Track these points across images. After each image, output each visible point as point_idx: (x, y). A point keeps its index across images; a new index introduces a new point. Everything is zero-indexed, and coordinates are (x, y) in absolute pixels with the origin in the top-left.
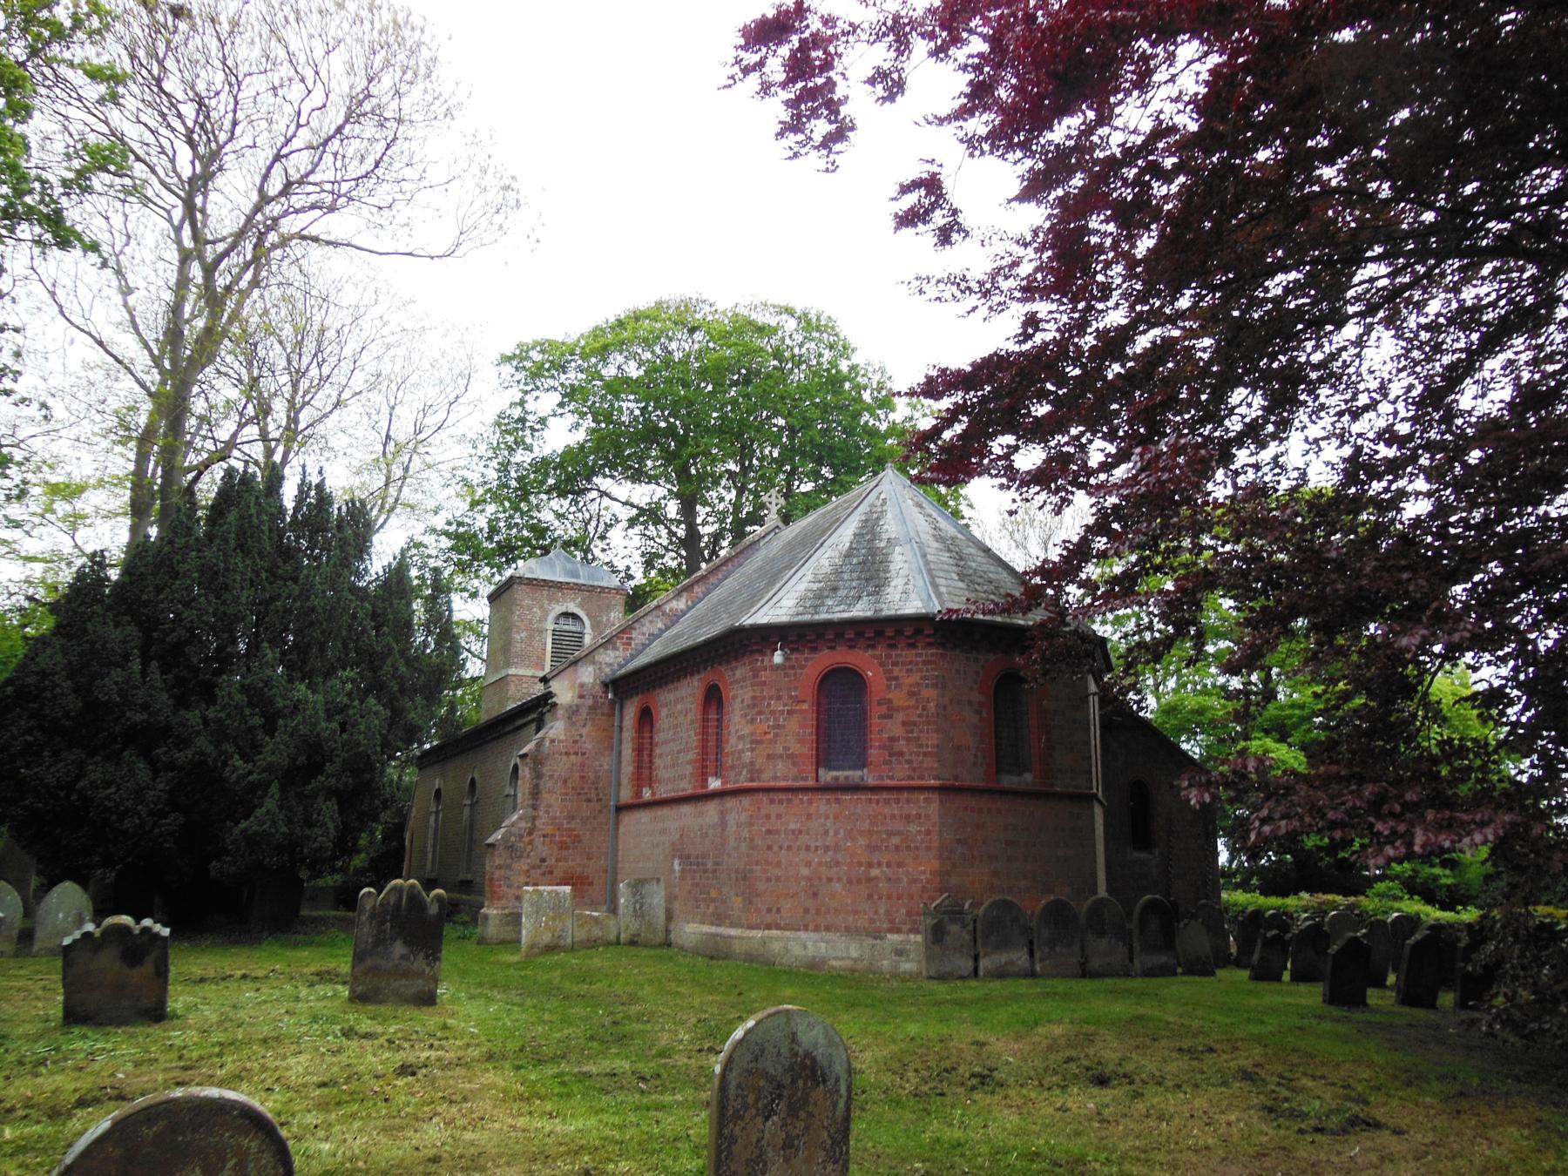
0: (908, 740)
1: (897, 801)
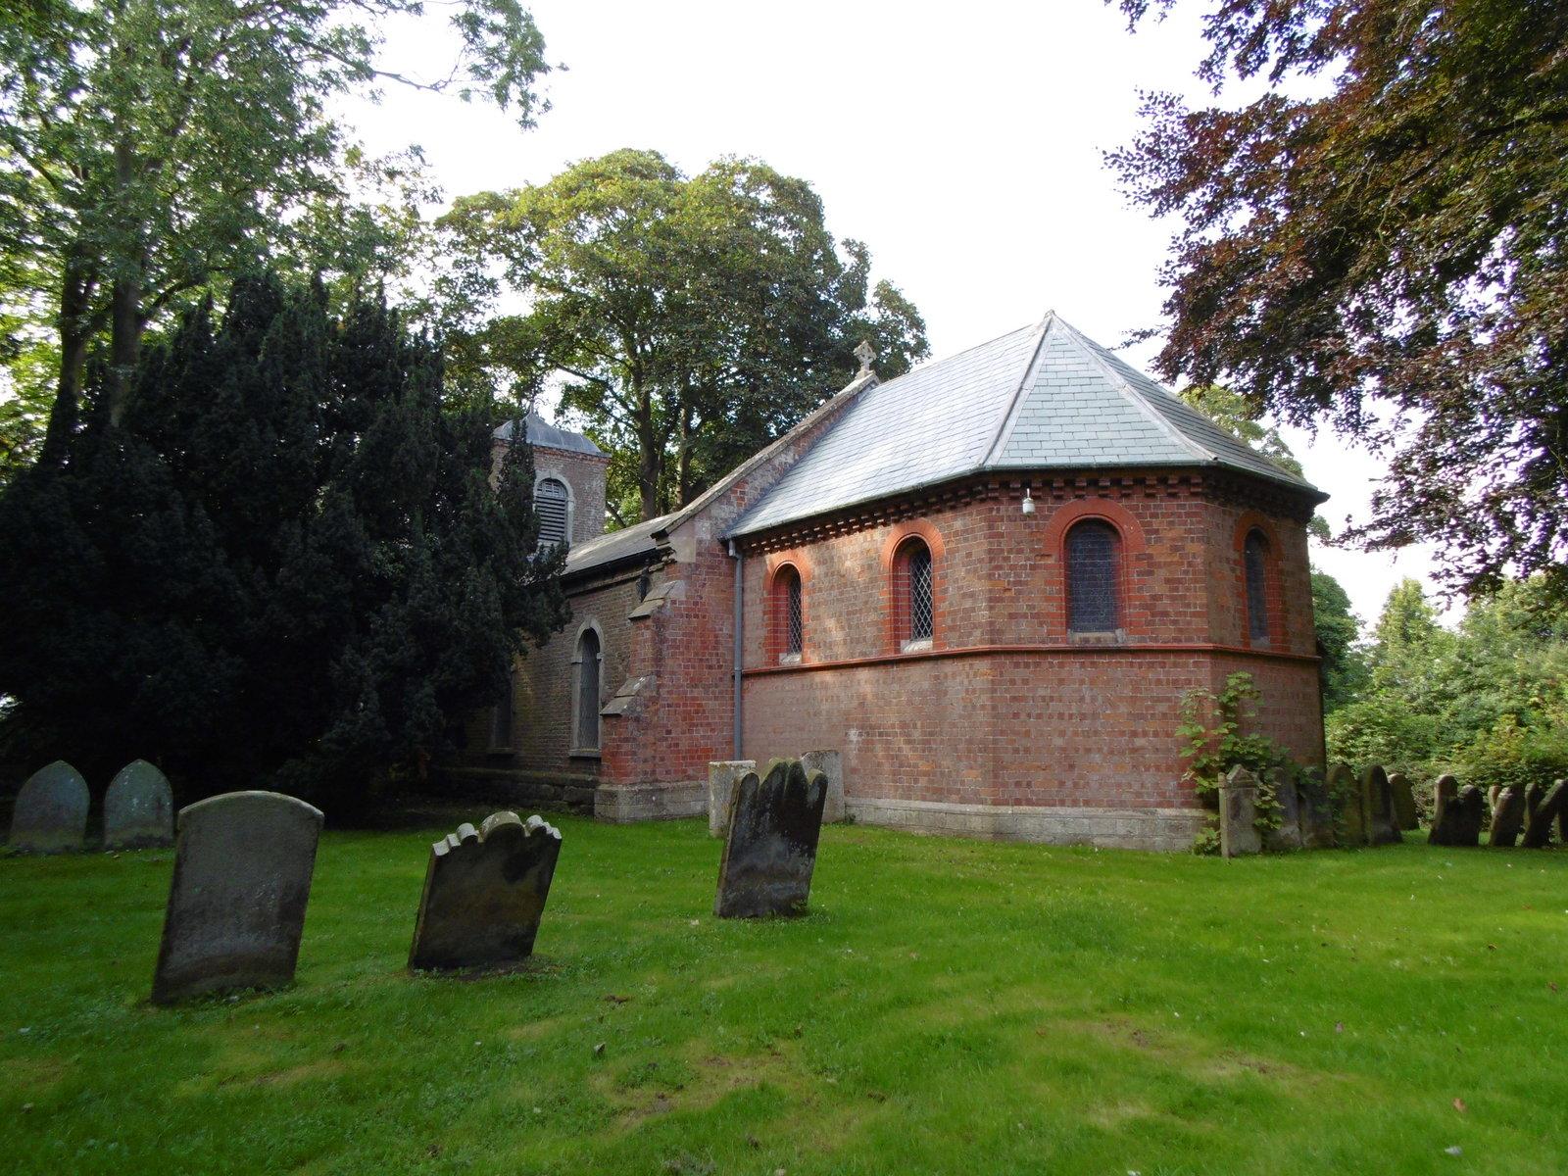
0: (1173, 598)
1: (1163, 665)
